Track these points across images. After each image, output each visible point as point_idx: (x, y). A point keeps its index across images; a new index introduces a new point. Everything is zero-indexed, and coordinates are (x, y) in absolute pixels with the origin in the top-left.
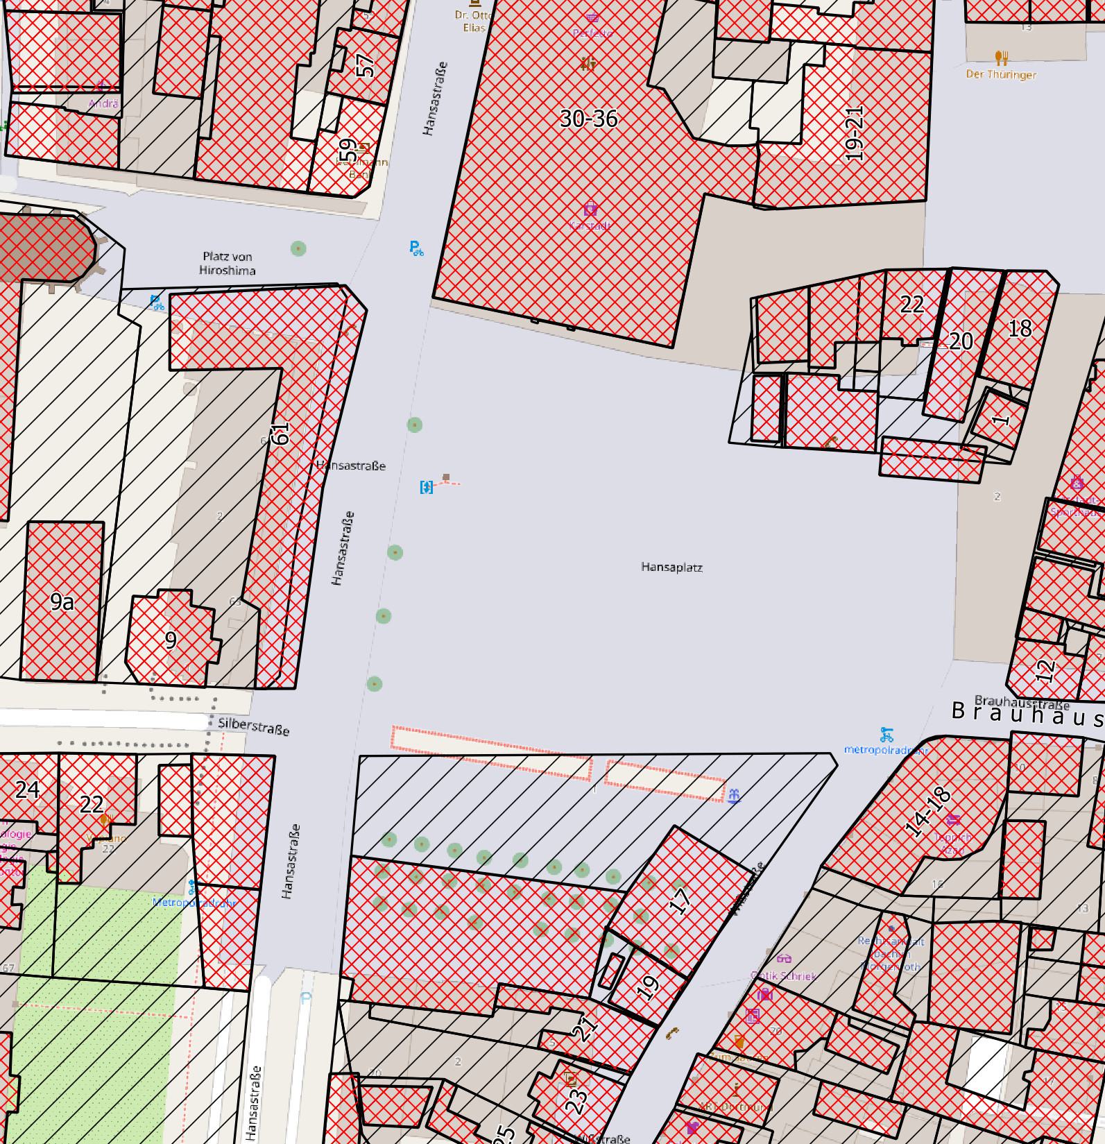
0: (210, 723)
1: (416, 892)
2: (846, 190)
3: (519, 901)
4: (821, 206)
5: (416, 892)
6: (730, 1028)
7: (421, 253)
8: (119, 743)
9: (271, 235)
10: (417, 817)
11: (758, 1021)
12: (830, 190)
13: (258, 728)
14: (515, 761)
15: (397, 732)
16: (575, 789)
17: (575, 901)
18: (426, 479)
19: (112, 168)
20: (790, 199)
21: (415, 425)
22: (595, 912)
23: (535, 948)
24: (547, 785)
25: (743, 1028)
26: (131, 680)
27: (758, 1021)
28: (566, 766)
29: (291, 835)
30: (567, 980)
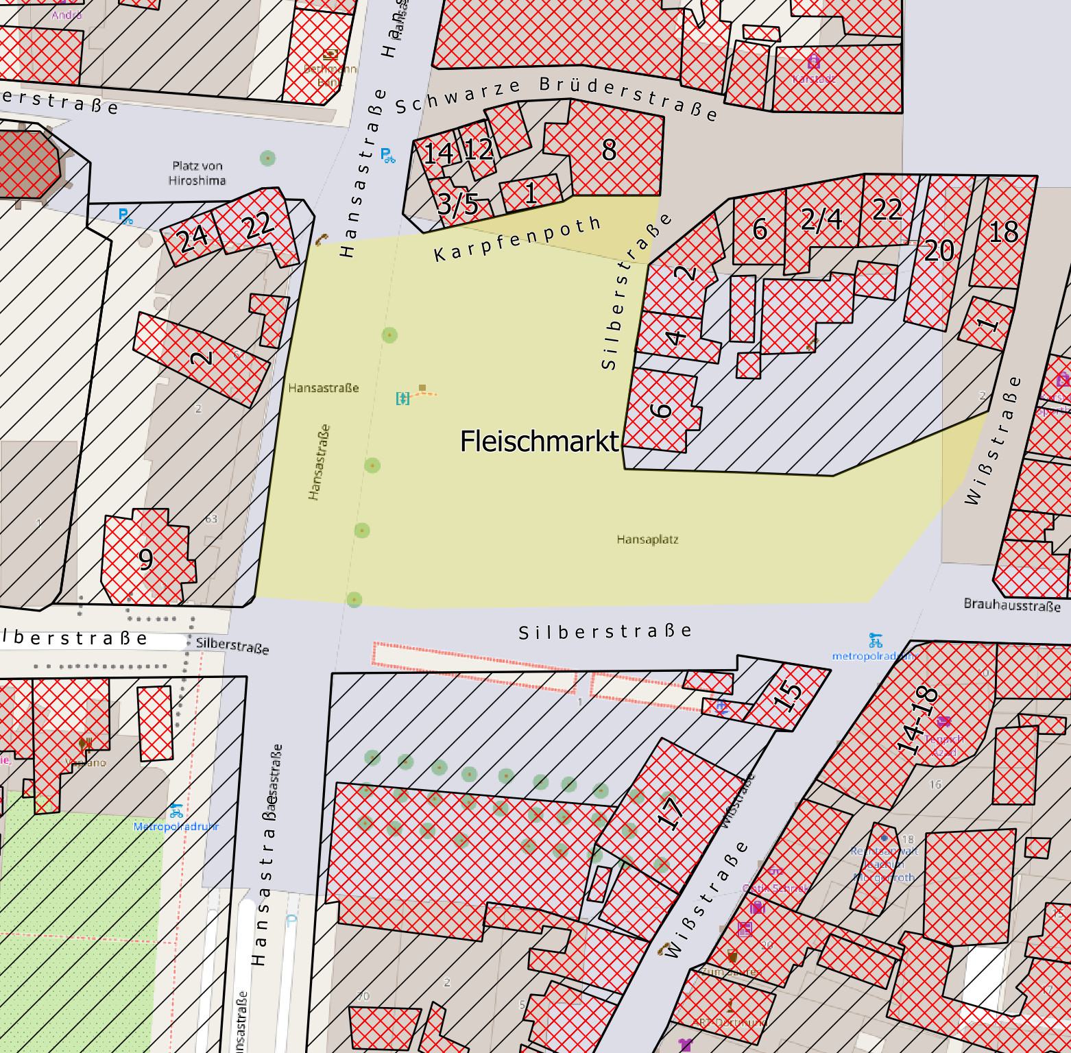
0: (188, 643)
1: (530, 832)
2: (554, 51)
3: (570, 824)
4: (528, 66)
5: (530, 832)
6: (722, 942)
7: (393, 161)
8: (105, 667)
9: (241, 150)
10: (412, 740)
11: (751, 935)
12: (538, 51)
13: (236, 646)
14: (512, 677)
15: (379, 648)
16: (570, 705)
17: (538, 816)
18: (404, 391)
19: (72, 85)
20: (467, 59)
21: (389, 335)
22: (582, 831)
23: (388, 847)
24: (543, 700)
25: (735, 942)
26: (103, 598)
27: (751, 935)
28: (620, 686)
29: (273, 755)
30: (530, 895)
